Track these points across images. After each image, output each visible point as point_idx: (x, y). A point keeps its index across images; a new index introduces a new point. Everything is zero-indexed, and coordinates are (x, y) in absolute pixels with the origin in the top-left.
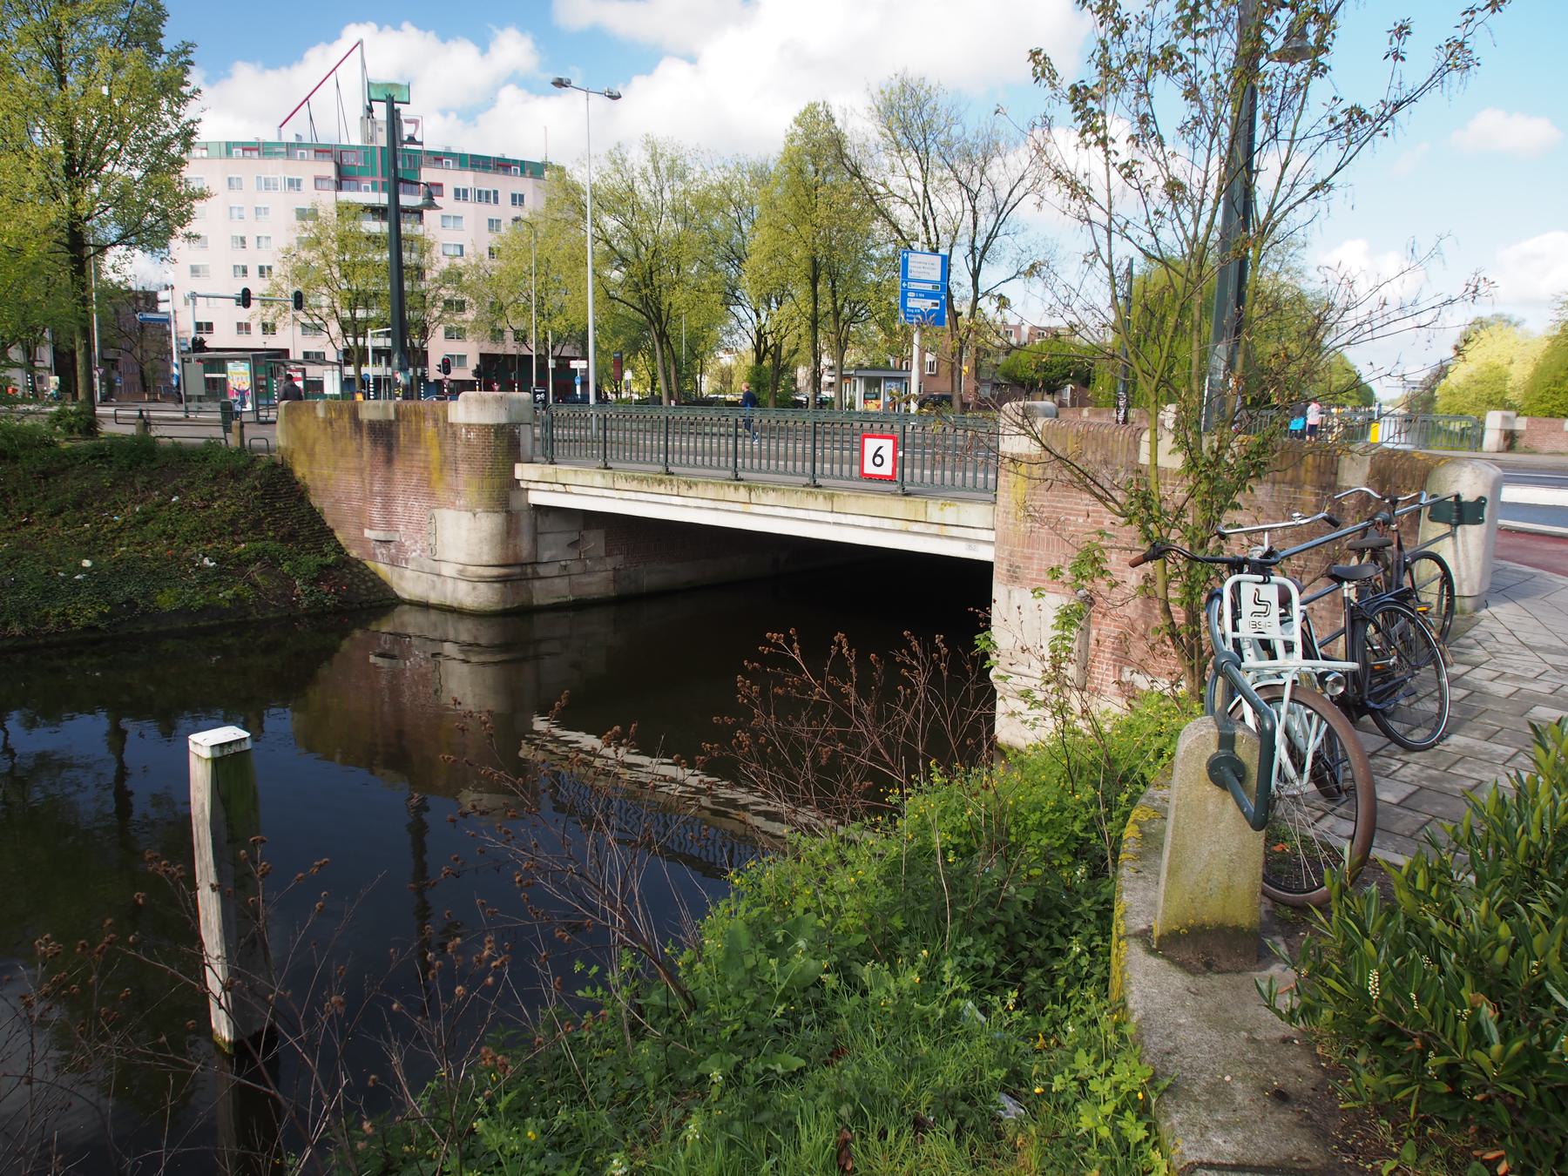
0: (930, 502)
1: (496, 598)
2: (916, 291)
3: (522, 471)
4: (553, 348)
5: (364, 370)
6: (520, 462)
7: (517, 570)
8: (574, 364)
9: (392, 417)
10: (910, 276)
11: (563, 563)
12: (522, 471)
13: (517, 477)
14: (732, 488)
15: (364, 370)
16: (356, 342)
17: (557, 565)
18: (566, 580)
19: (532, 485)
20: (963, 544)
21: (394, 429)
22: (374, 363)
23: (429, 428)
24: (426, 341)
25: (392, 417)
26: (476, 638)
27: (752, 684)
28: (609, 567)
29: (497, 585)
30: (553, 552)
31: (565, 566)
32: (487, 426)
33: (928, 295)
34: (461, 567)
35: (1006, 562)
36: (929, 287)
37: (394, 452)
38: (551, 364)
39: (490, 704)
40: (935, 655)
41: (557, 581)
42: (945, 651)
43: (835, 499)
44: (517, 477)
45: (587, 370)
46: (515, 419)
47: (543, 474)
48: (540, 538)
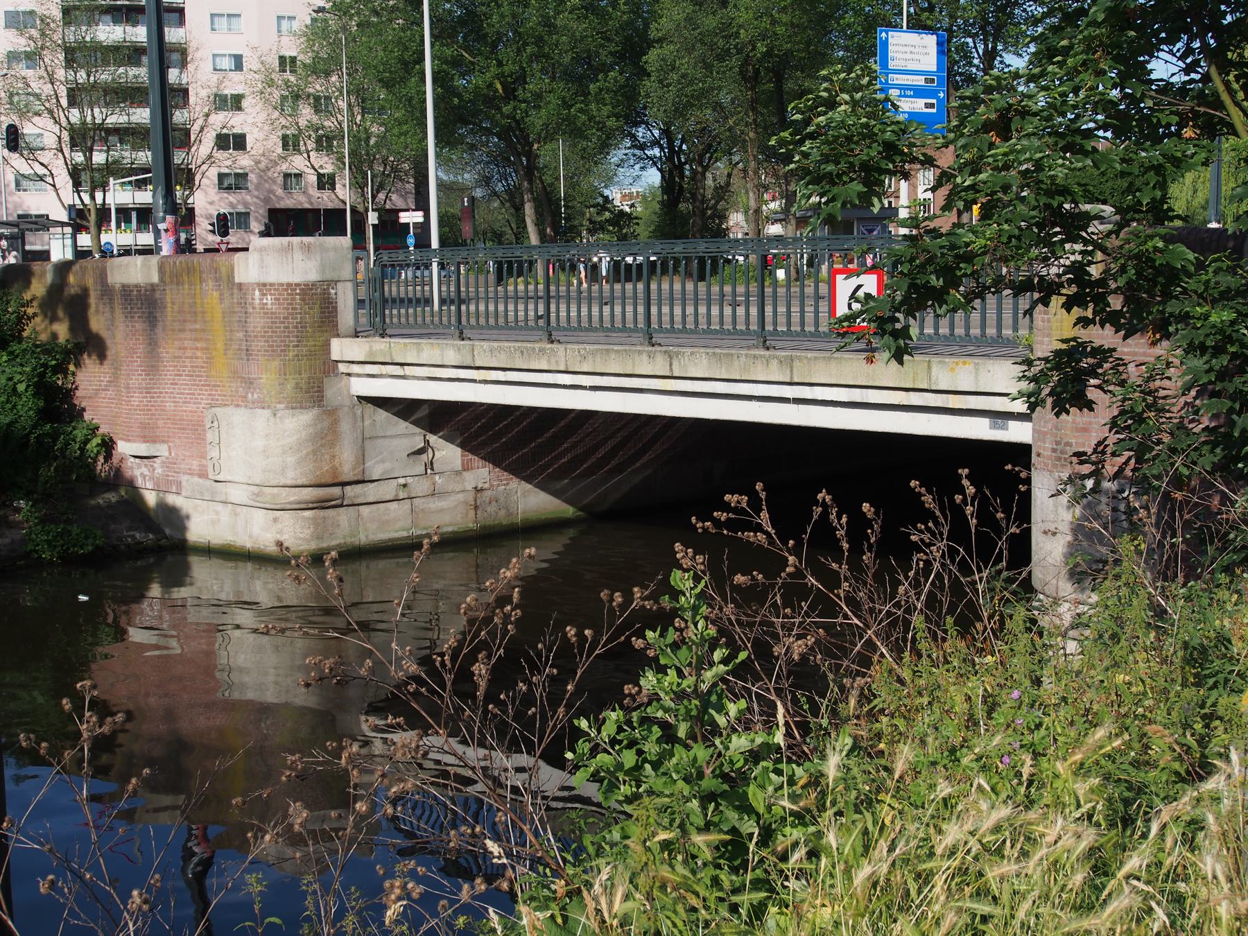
0: (935, 360)
1: (307, 533)
2: (902, 88)
3: (340, 348)
4: (374, 197)
5: (105, 238)
6: (338, 336)
7: (336, 491)
8: (405, 218)
9: (155, 279)
10: (891, 65)
11: (402, 481)
12: (340, 348)
13: (335, 356)
14: (645, 357)
15: (105, 238)
16: (93, 198)
17: (394, 482)
18: (406, 505)
19: (356, 369)
20: (985, 422)
21: (157, 295)
22: (118, 226)
23: (211, 296)
24: (192, 193)
25: (155, 279)
26: (279, 599)
27: (695, 554)
28: (469, 487)
29: (307, 513)
30: (388, 465)
31: (405, 486)
32: (289, 285)
33: (918, 92)
34: (255, 489)
35: (1049, 438)
36: (920, 81)
37: (159, 330)
38: (373, 218)
39: (303, 698)
40: (958, 498)
41: (394, 505)
42: (971, 490)
43: (796, 364)
44: (335, 356)
45: (425, 226)
46: (329, 276)
47: (371, 353)
48: (367, 442)
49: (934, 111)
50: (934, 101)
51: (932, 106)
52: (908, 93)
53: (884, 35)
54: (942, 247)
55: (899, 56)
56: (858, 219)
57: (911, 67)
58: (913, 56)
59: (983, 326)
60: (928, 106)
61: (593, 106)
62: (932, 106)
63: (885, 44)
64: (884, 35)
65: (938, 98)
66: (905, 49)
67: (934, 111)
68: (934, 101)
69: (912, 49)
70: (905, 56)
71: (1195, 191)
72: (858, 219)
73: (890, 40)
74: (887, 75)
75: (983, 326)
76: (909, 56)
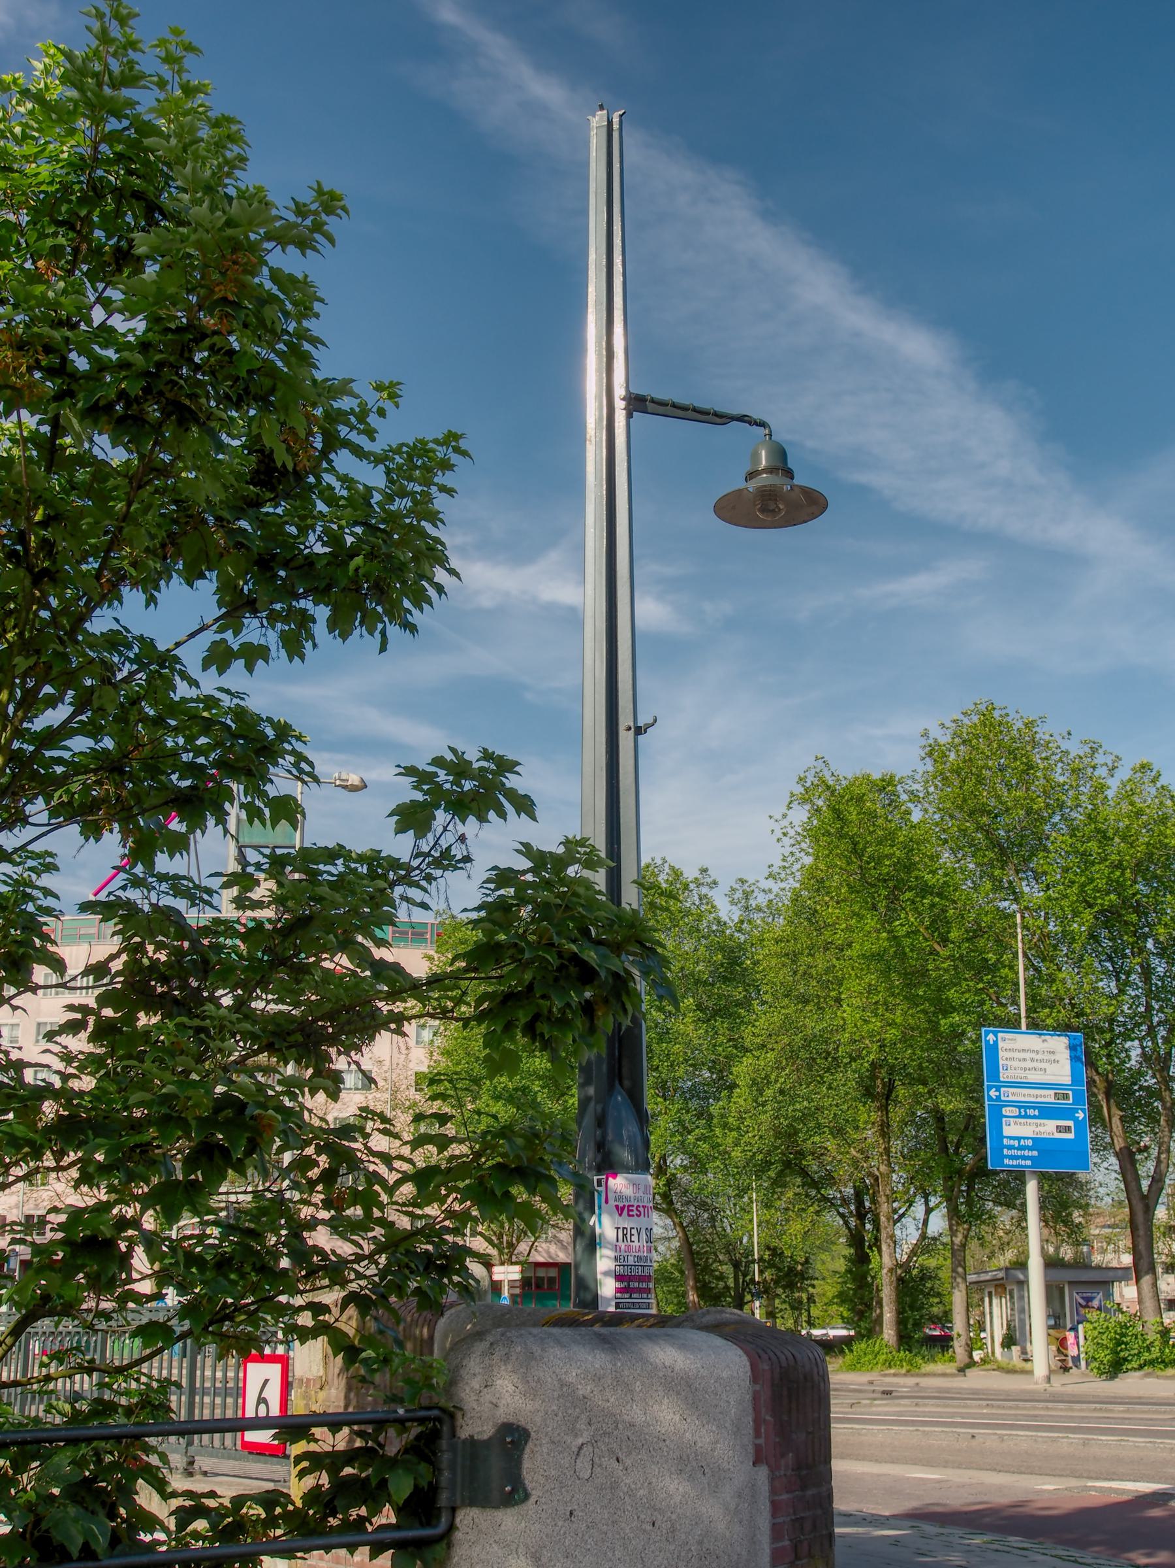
36: (1048, 1097)
49: (1071, 1136)
50: (1070, 1123)
51: (1067, 1129)
52: (1031, 1112)
53: (991, 1037)
54: (884, 1130)
55: (1015, 1064)
56: (1070, 1283)
57: (1033, 1077)
58: (1035, 1064)
59: (161, 1368)
60: (1060, 1129)
61: (718, 1131)
62: (1067, 1129)
63: (994, 1048)
64: (991, 1037)
65: (1076, 1120)
66: (1022, 1055)
67: (1071, 1136)
68: (1070, 1123)
69: (1034, 1055)
70: (1023, 1064)
71: (580, 1448)
72: (1070, 1283)
73: (1001, 1044)
74: (998, 1089)
75: (161, 1368)
76: (1029, 1064)
